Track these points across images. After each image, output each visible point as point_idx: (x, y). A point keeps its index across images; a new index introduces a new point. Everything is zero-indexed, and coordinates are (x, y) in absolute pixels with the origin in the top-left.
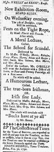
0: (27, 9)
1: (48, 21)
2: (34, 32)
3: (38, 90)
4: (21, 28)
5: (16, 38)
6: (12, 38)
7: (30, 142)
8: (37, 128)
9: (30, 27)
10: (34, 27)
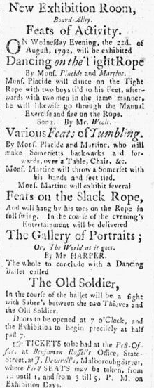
3: (64, 10)
4: (60, 194)
8: (84, 131)
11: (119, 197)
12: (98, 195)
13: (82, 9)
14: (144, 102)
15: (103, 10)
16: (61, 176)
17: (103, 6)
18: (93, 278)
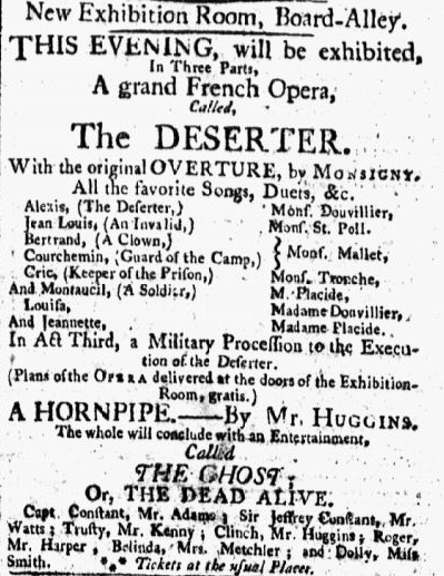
3: (55, 41)
6: (101, 79)
12: (246, 84)
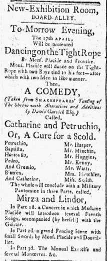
0: (56, 8)
1: (94, 33)
2: (74, 58)
5: (65, 143)
6: (28, 89)
7: (72, 217)
9: (65, 48)
10: (55, 120)
11: (79, 10)
12: (86, 125)
13: (60, 10)
14: (73, 42)
15: (76, 11)
16: (29, 235)
17: (76, 8)
18: (87, 133)
